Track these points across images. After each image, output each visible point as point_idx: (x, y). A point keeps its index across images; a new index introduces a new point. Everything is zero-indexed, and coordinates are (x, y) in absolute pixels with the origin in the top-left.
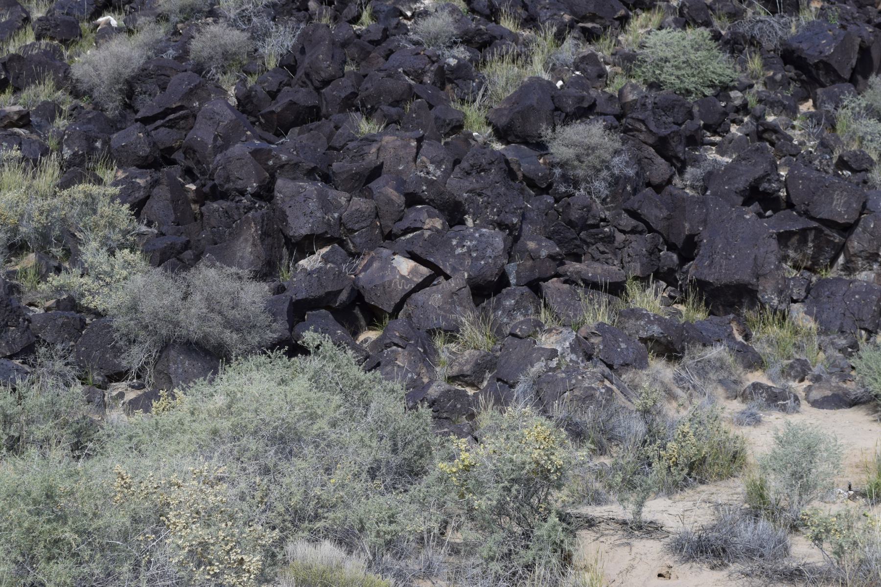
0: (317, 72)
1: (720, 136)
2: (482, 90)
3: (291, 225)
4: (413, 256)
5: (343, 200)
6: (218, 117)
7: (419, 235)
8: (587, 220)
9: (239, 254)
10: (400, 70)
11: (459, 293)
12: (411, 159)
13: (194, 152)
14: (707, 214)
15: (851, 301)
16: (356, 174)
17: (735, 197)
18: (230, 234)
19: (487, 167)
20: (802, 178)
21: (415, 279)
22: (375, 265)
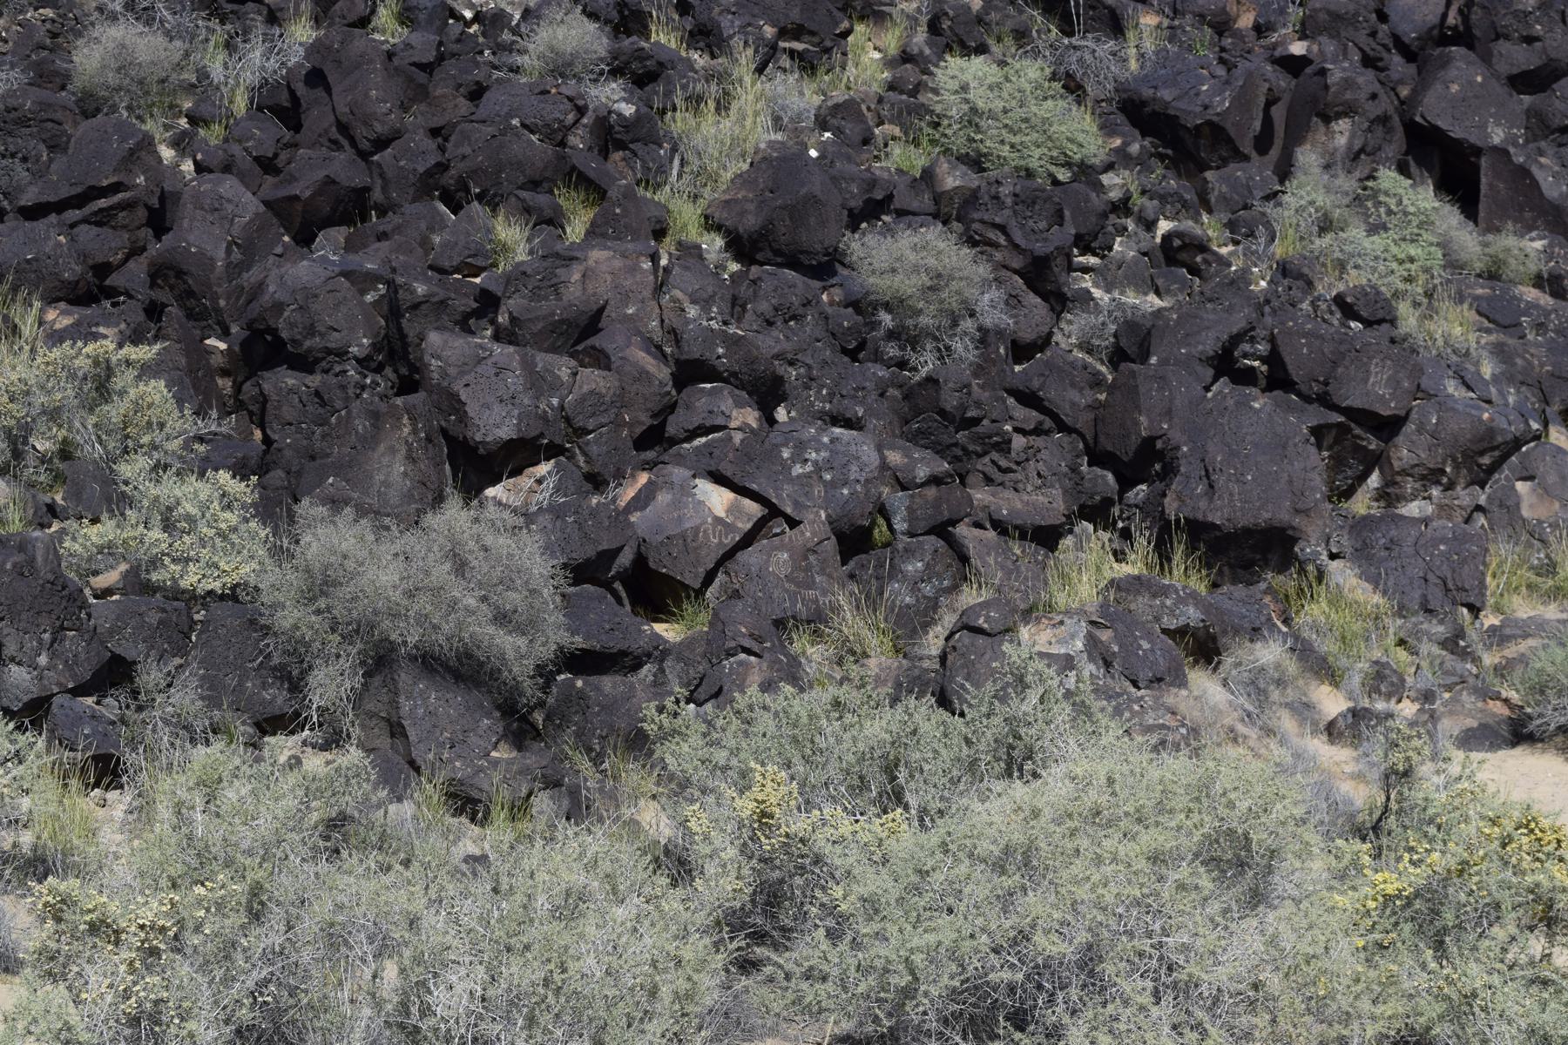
0: (365, 123)
1: (1095, 254)
2: (676, 162)
3: (477, 422)
4: (720, 479)
5: (564, 374)
6: (230, 208)
7: (721, 440)
8: (966, 409)
9: (379, 477)
10: (515, 122)
11: (819, 549)
12: (647, 293)
13: (180, 274)
14: (1171, 400)
15: (1432, 555)
16: (562, 321)
17: (1199, 368)
18: (324, 436)
19: (800, 311)
20: (1306, 335)
21: (740, 525)
22: (663, 498)
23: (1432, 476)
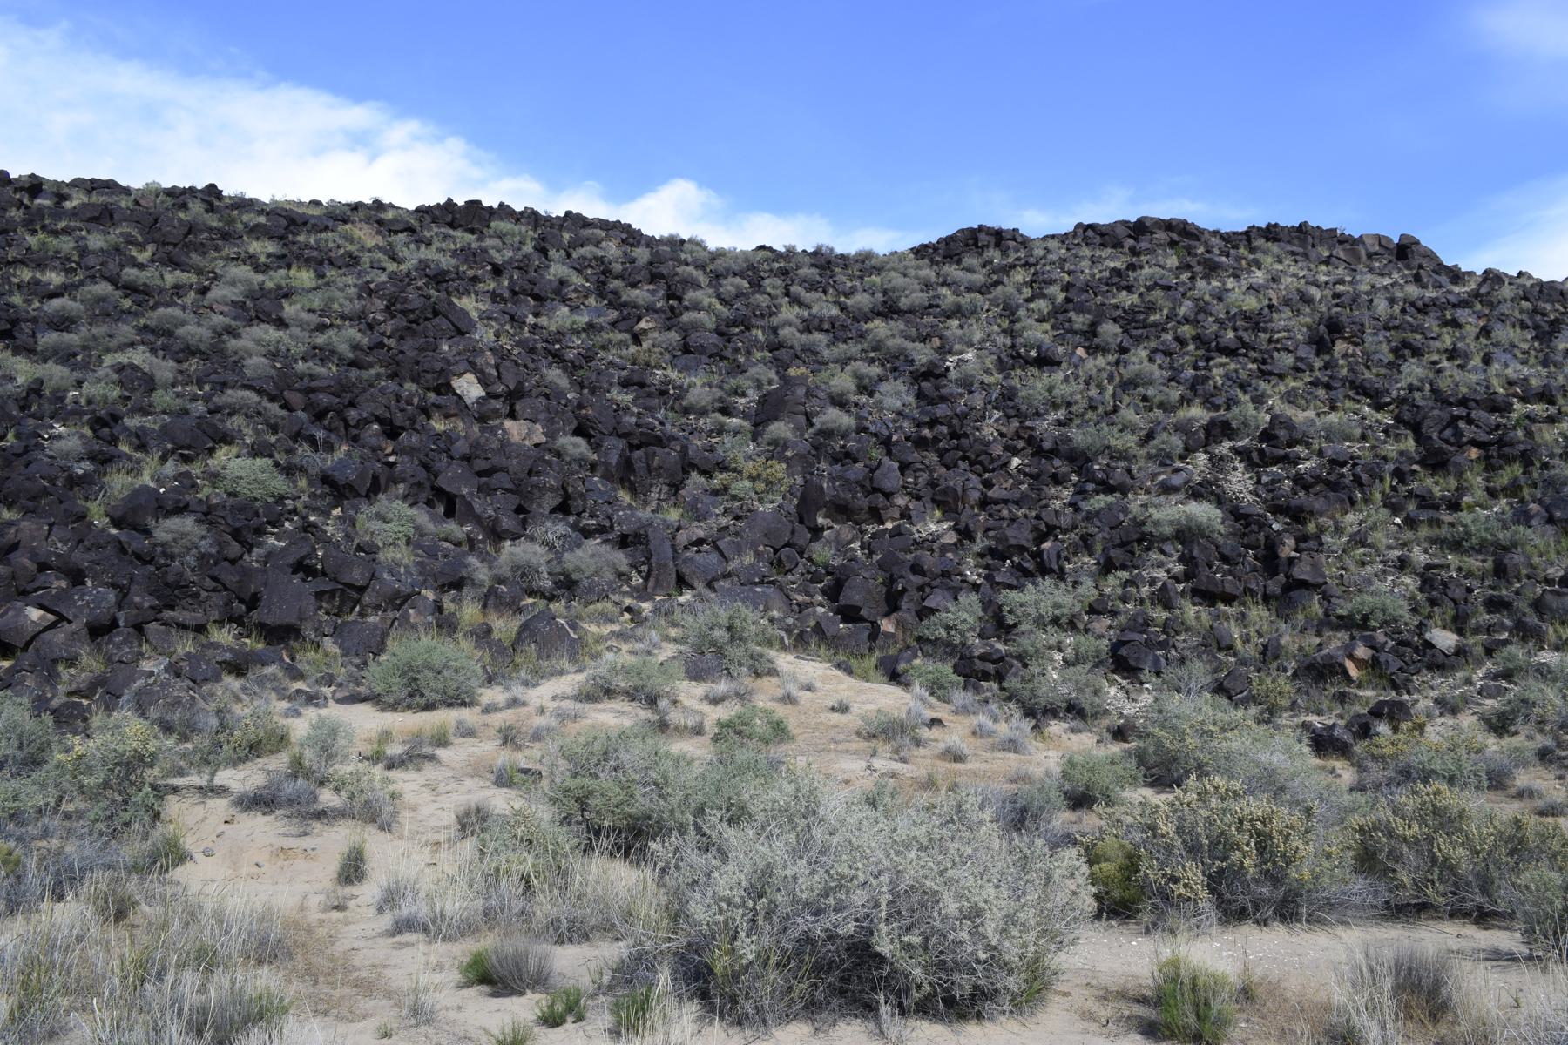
23: (377, 607)
